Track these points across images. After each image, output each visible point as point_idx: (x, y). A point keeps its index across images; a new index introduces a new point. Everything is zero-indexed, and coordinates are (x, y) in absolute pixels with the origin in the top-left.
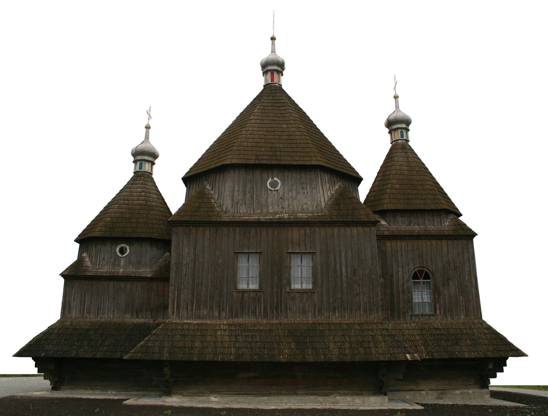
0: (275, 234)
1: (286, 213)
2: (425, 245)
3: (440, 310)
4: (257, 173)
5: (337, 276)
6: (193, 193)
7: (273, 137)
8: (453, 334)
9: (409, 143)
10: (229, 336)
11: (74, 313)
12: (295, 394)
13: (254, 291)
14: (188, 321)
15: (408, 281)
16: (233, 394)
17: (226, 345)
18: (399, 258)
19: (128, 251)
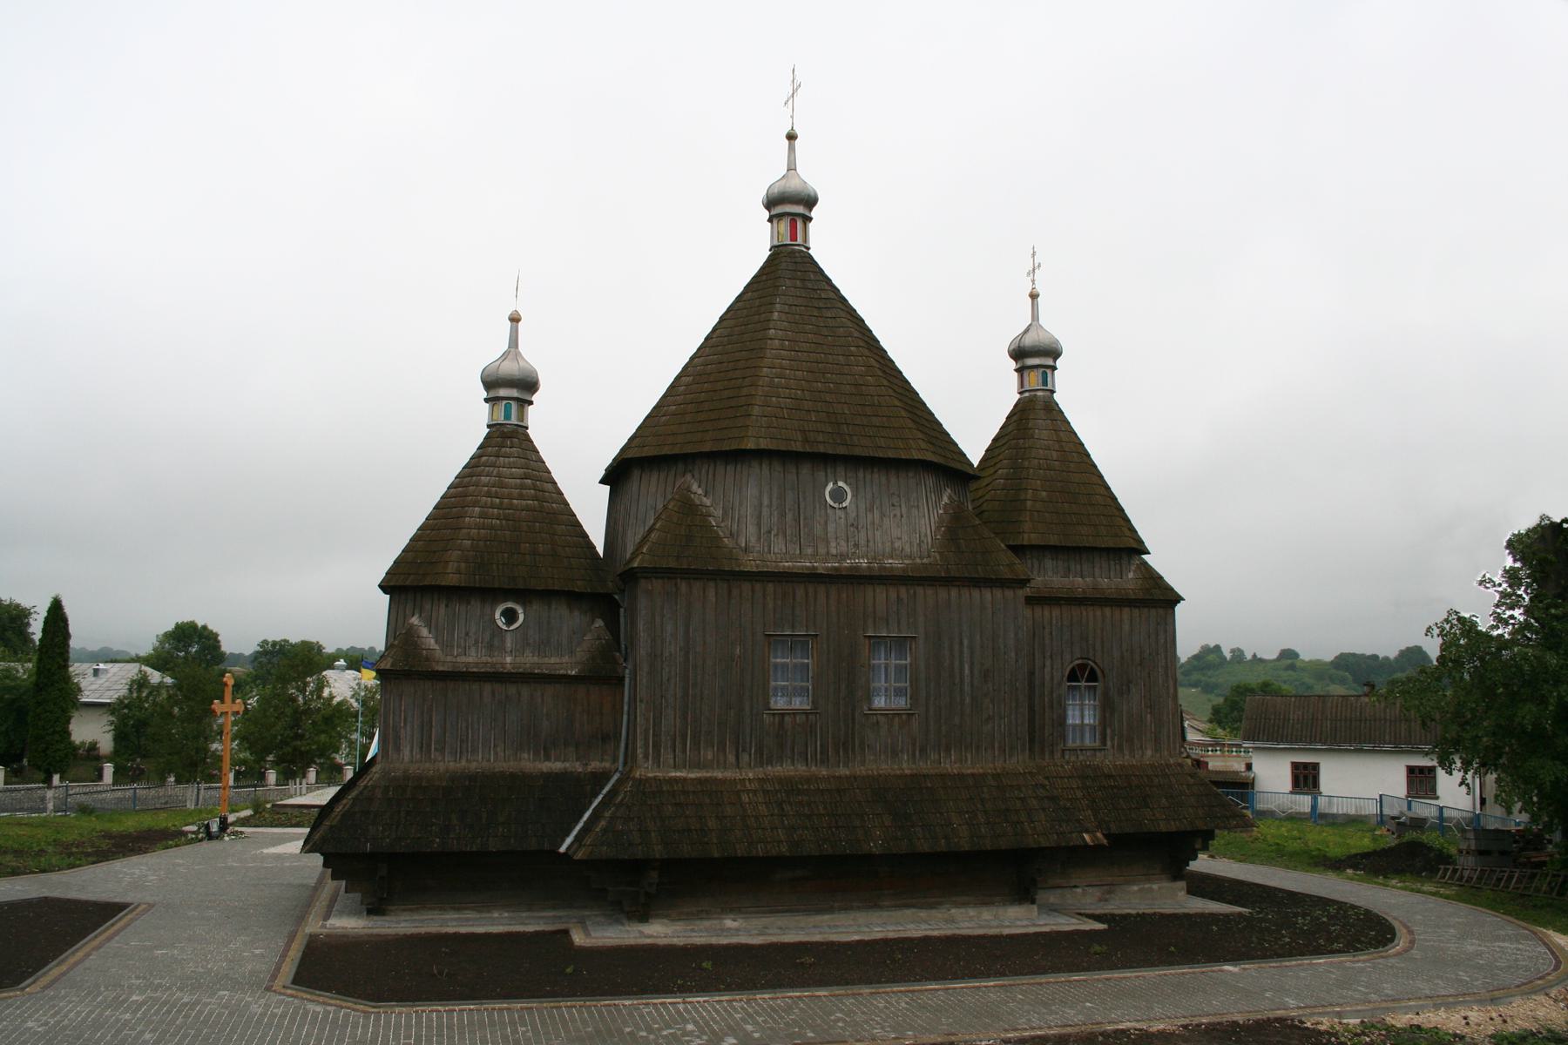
2: (1093, 616)
4: (805, 470)
7: (788, 368)
12: (875, 906)
15: (1060, 684)
18: (1047, 641)
19: (521, 617)
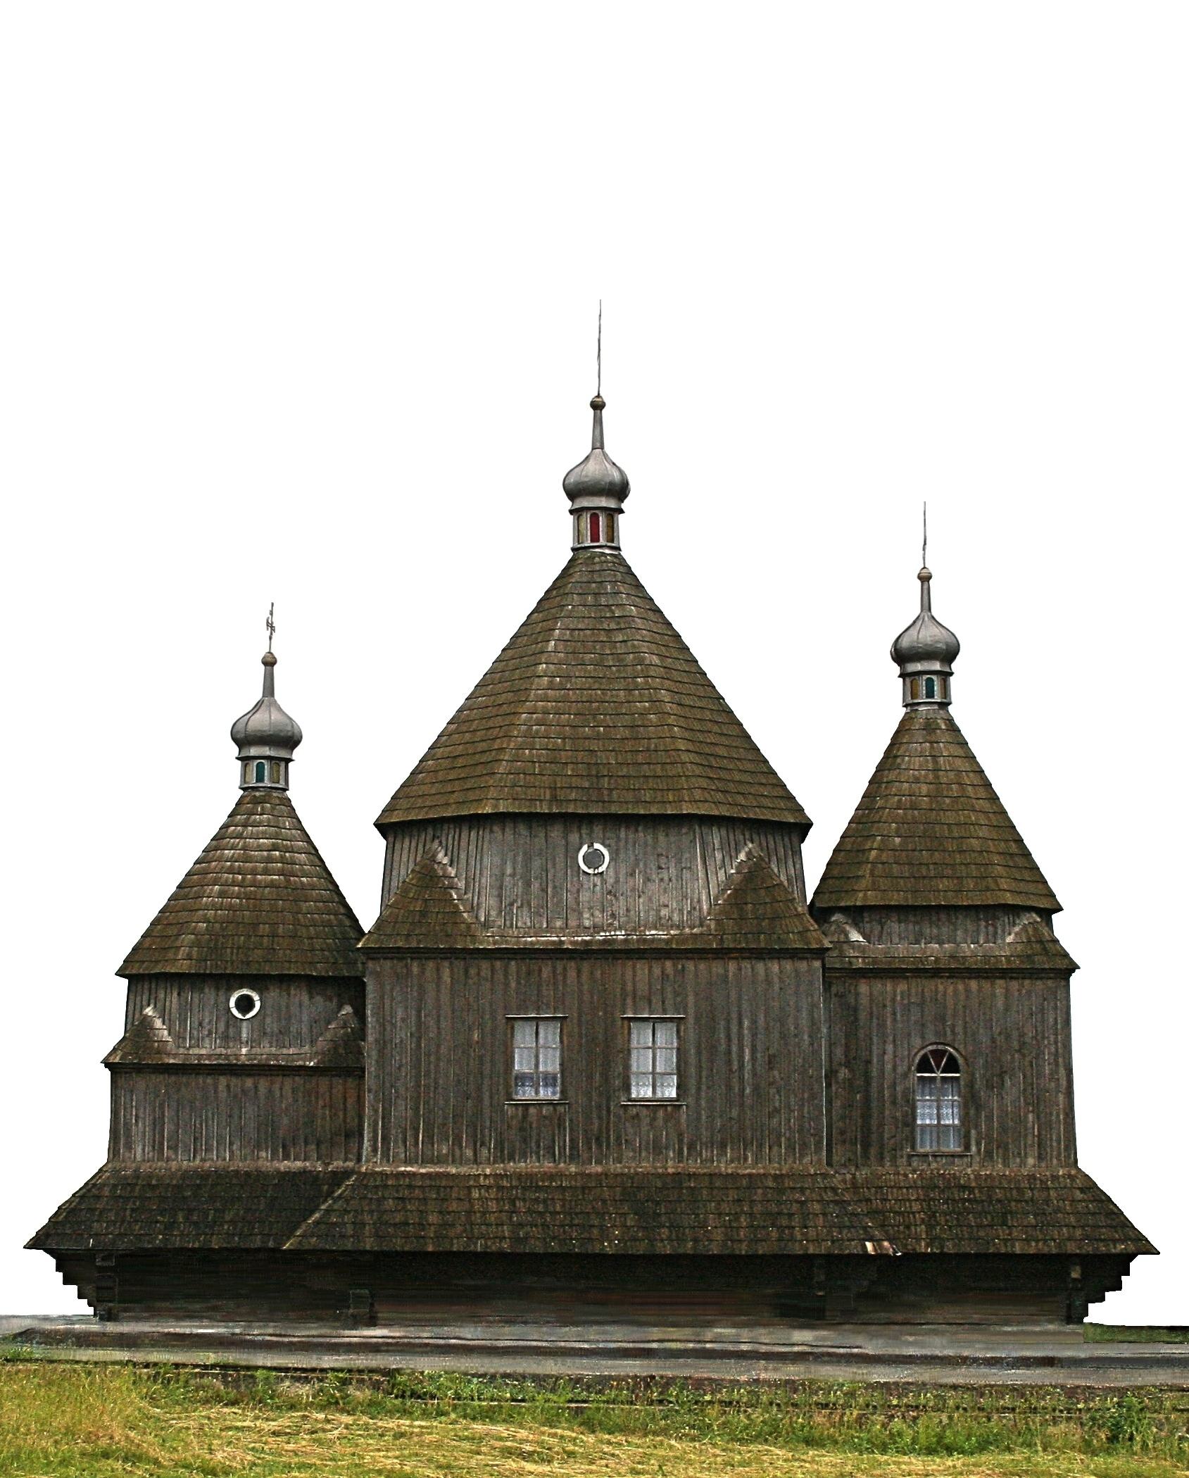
0: (595, 980)
1: (620, 929)
2: (948, 989)
3: (978, 1144)
4: (556, 832)
5: (731, 1070)
6: (404, 871)
7: (594, 711)
8: (999, 1201)
10: (497, 1199)
11: (139, 1150)
13: (550, 1103)
14: (409, 1169)
15: (905, 1076)
17: (492, 1219)
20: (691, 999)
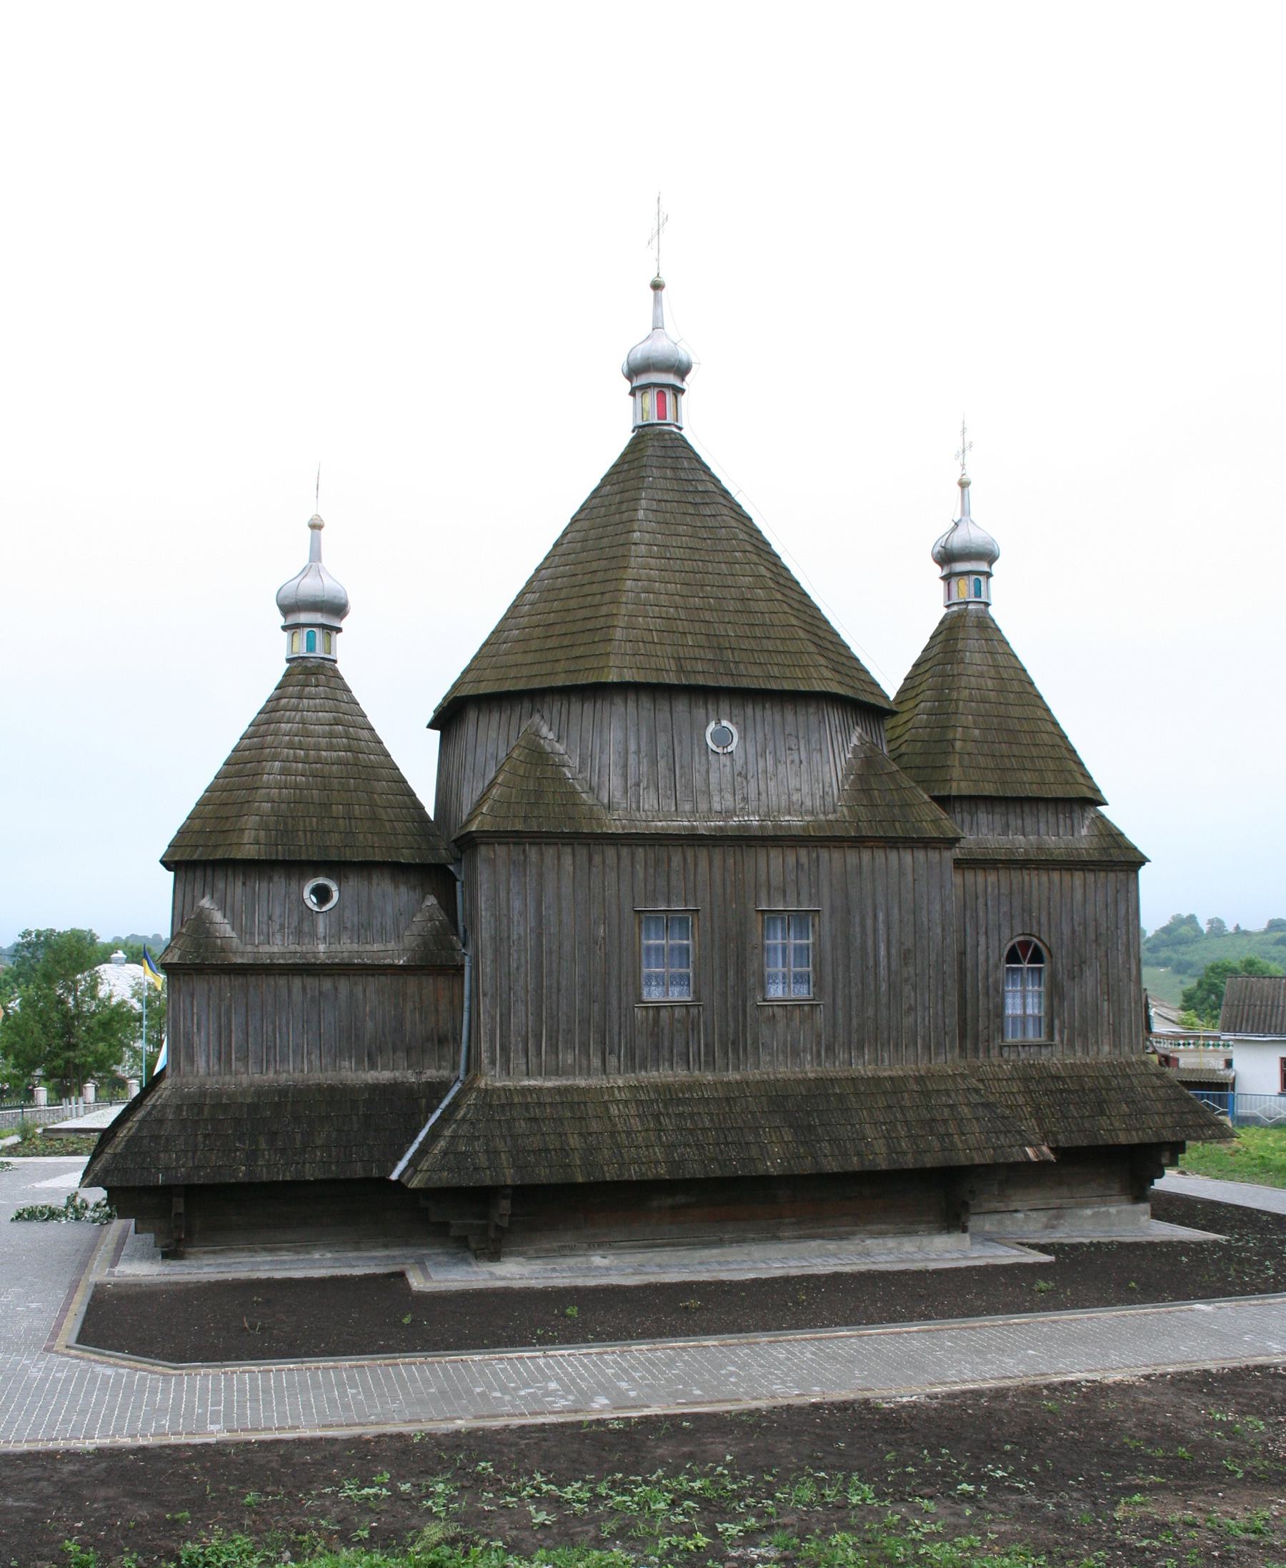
1: (753, 814)
2: (1037, 882)
3: (1061, 1033)
4: (681, 706)
8: (1092, 1090)
9: (991, 610)
10: (639, 1116)
14: (532, 1083)
15: (997, 967)
16: (640, 1247)
20: (825, 890)
